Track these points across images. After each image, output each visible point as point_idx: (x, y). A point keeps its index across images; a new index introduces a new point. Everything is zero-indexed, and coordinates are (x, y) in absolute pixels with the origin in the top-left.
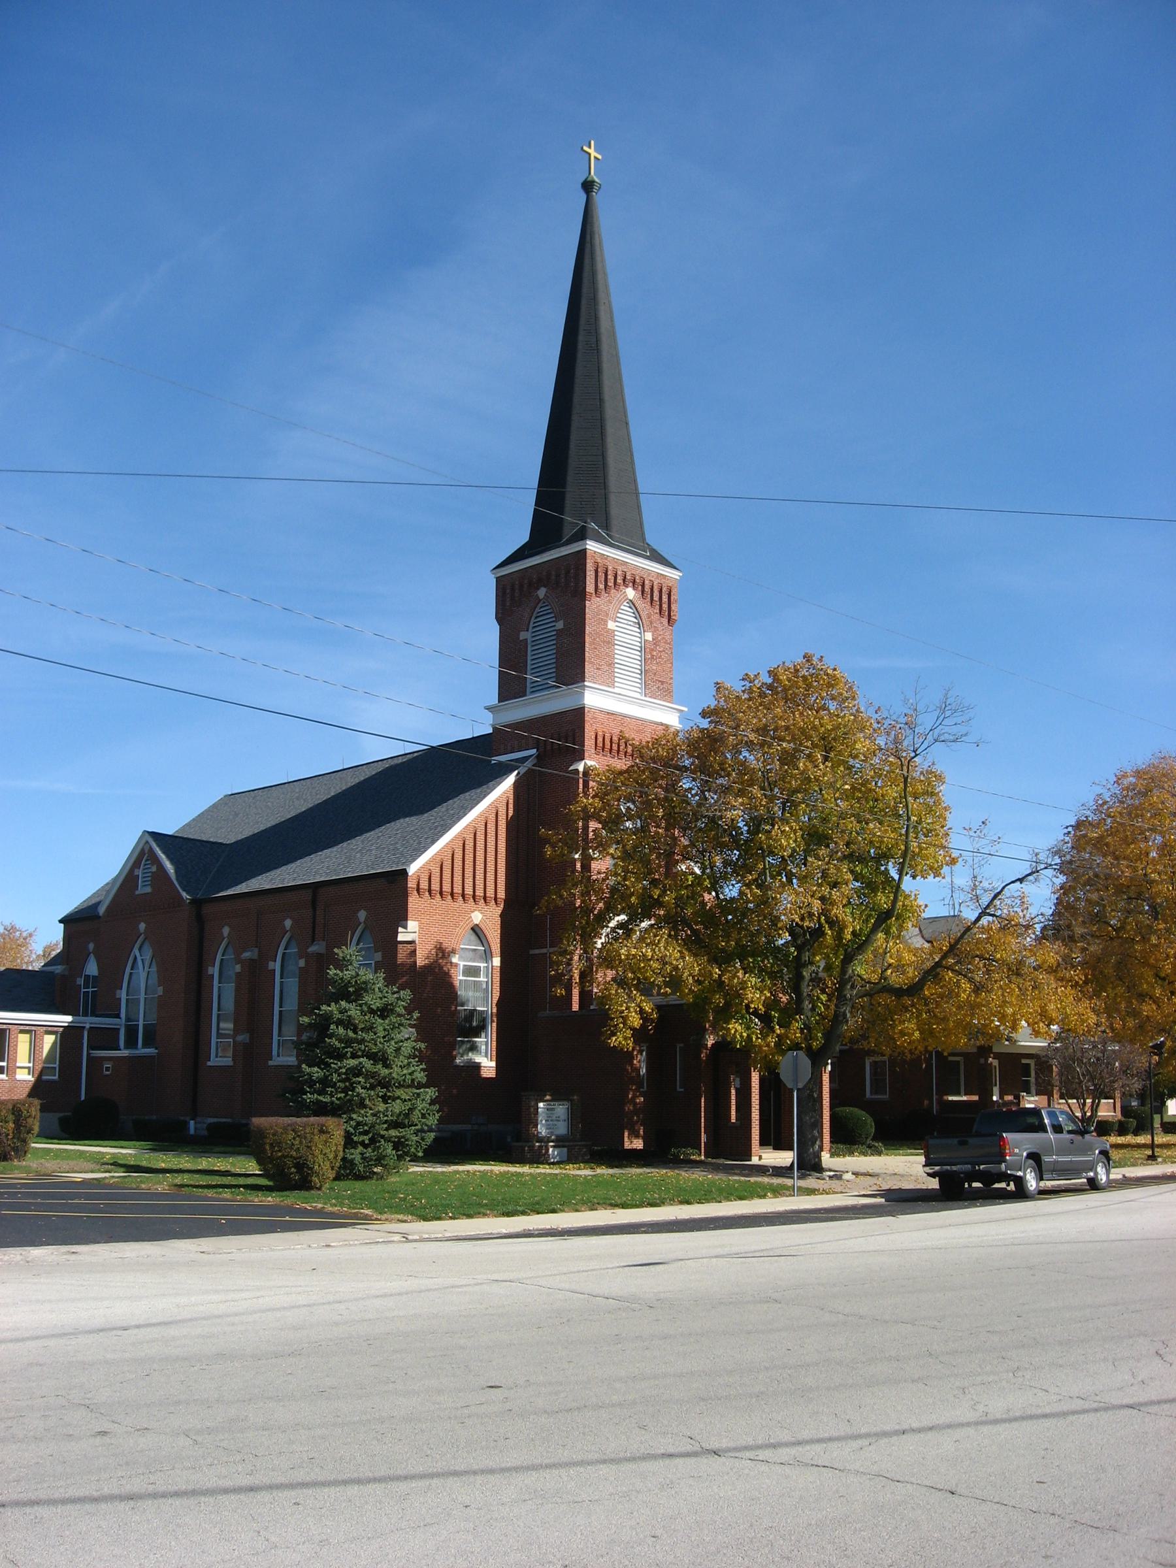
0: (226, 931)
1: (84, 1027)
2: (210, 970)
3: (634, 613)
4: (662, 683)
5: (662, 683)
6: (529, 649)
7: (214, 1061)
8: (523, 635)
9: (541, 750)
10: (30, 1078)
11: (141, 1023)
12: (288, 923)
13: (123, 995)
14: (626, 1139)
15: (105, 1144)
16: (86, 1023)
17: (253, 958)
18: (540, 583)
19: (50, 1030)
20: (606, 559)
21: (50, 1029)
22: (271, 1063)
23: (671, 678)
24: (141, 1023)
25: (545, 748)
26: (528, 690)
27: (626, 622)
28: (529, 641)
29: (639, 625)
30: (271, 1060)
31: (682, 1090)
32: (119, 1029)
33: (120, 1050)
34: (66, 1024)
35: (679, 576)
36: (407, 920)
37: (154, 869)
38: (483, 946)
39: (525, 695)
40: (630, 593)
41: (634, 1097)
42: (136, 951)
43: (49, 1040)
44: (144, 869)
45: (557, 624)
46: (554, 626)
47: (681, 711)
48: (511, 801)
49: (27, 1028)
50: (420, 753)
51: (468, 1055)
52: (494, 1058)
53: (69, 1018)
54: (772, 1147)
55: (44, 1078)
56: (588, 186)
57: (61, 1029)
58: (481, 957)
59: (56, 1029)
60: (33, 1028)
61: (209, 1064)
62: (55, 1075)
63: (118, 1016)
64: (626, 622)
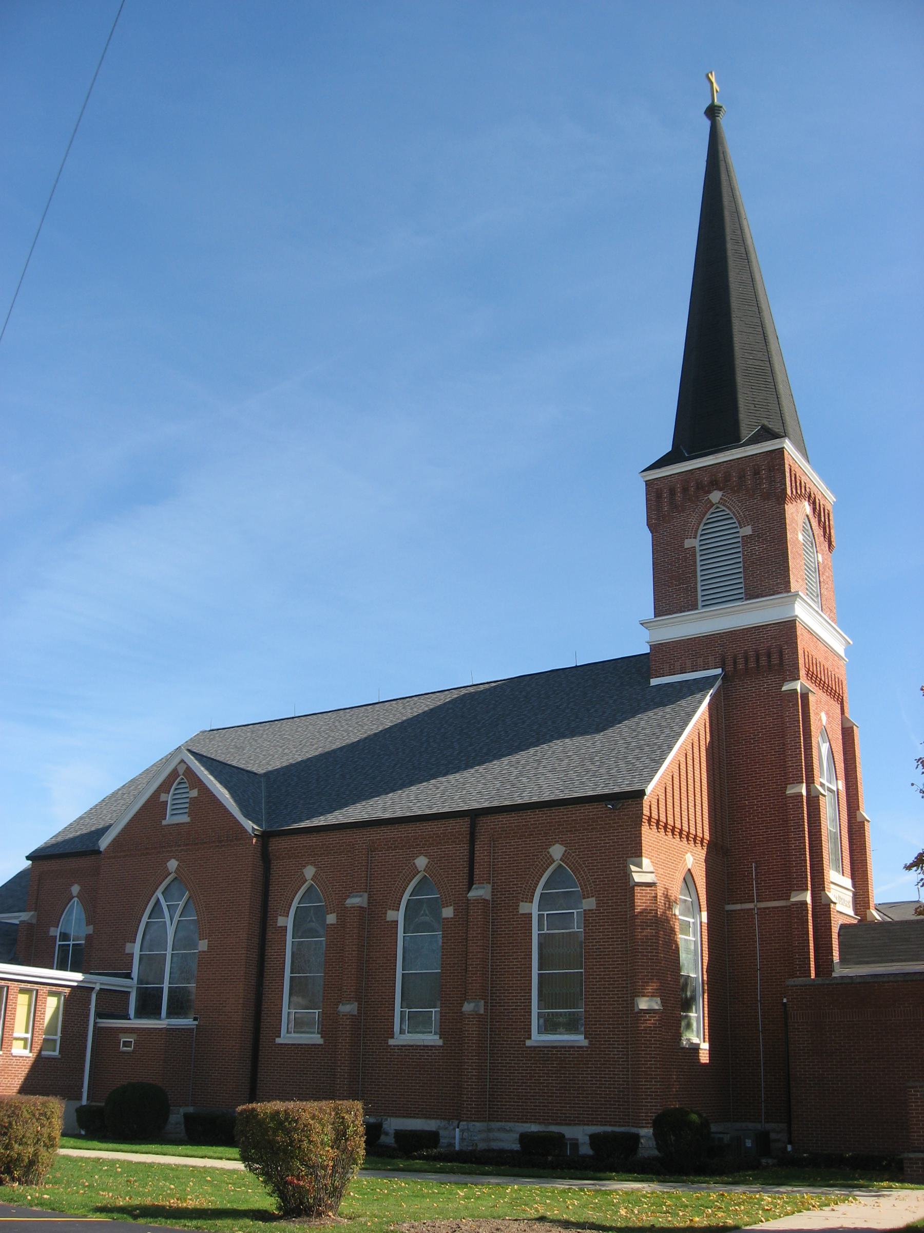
0: (309, 872)
1: (94, 988)
2: (281, 921)
6: (698, 558)
7: (287, 1036)
8: (688, 543)
9: (730, 668)
10: (26, 1053)
11: (166, 986)
12: (421, 862)
13: (136, 949)
15: (200, 1154)
16: (95, 983)
17: (363, 905)
18: (714, 484)
19: (54, 989)
21: (54, 988)
22: (391, 1042)
24: (166, 986)
25: (735, 668)
26: (700, 604)
28: (698, 549)
29: (812, 544)
30: (393, 1038)
32: (129, 992)
33: (130, 1019)
34: (75, 984)
36: (641, 856)
37: (194, 793)
39: (697, 609)
42: (159, 894)
43: (52, 1004)
44: (175, 794)
45: (741, 530)
46: (738, 532)
48: (708, 724)
49: (29, 986)
50: (487, 686)
52: (707, 1039)
53: (79, 976)
56: (712, 112)
57: (67, 990)
59: (61, 989)
60: (36, 987)
61: (278, 1041)
62: (54, 1051)
63: (128, 976)
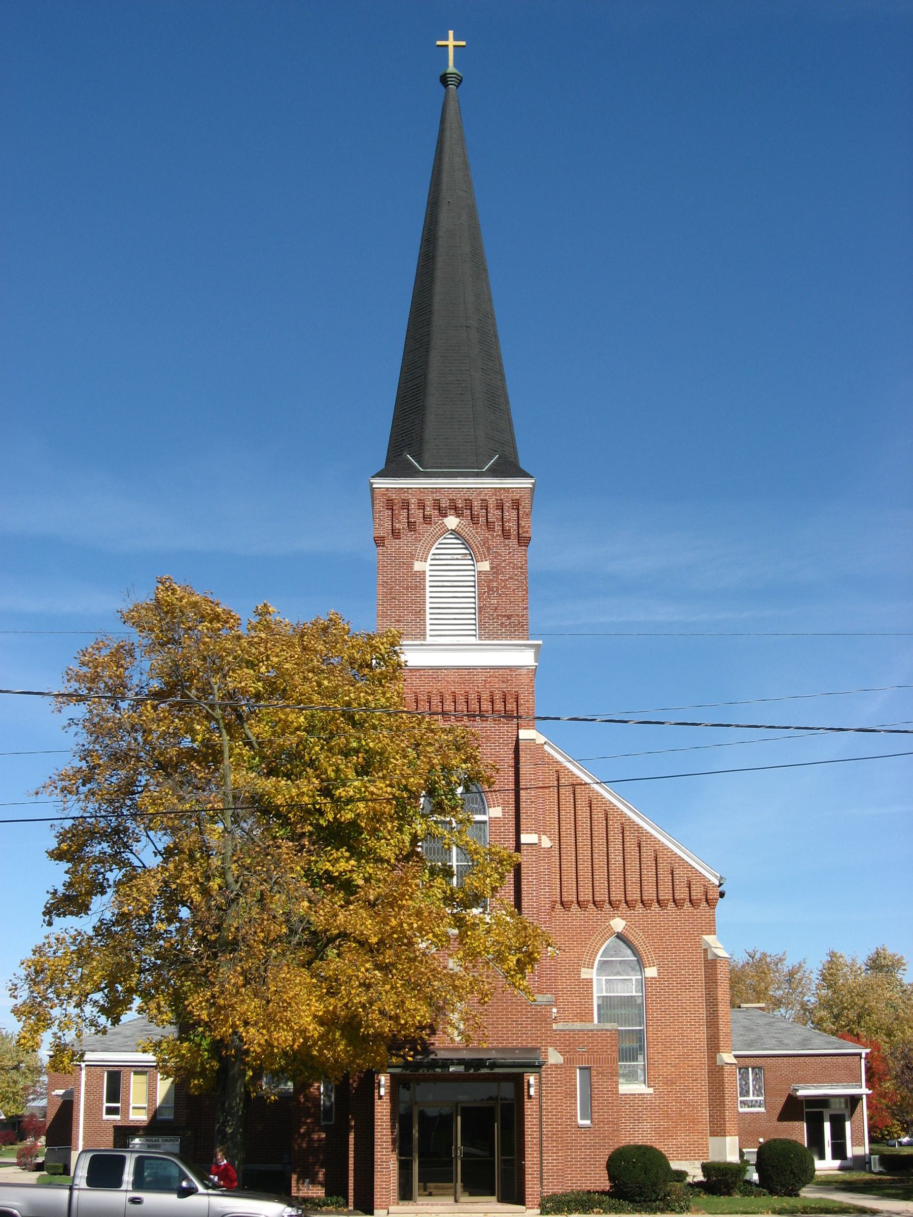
3: (462, 544)
4: (509, 617)
5: (509, 617)
14: (294, 1183)
20: (404, 492)
21: (140, 1069)
23: (526, 608)
27: (449, 557)
31: (588, 1122)
35: (532, 484)
38: (636, 957)
40: (452, 522)
41: (308, 1133)
47: (536, 646)
51: (286, 1085)
54: (494, 1198)
55: (160, 1117)
58: (633, 969)
64: (449, 557)
